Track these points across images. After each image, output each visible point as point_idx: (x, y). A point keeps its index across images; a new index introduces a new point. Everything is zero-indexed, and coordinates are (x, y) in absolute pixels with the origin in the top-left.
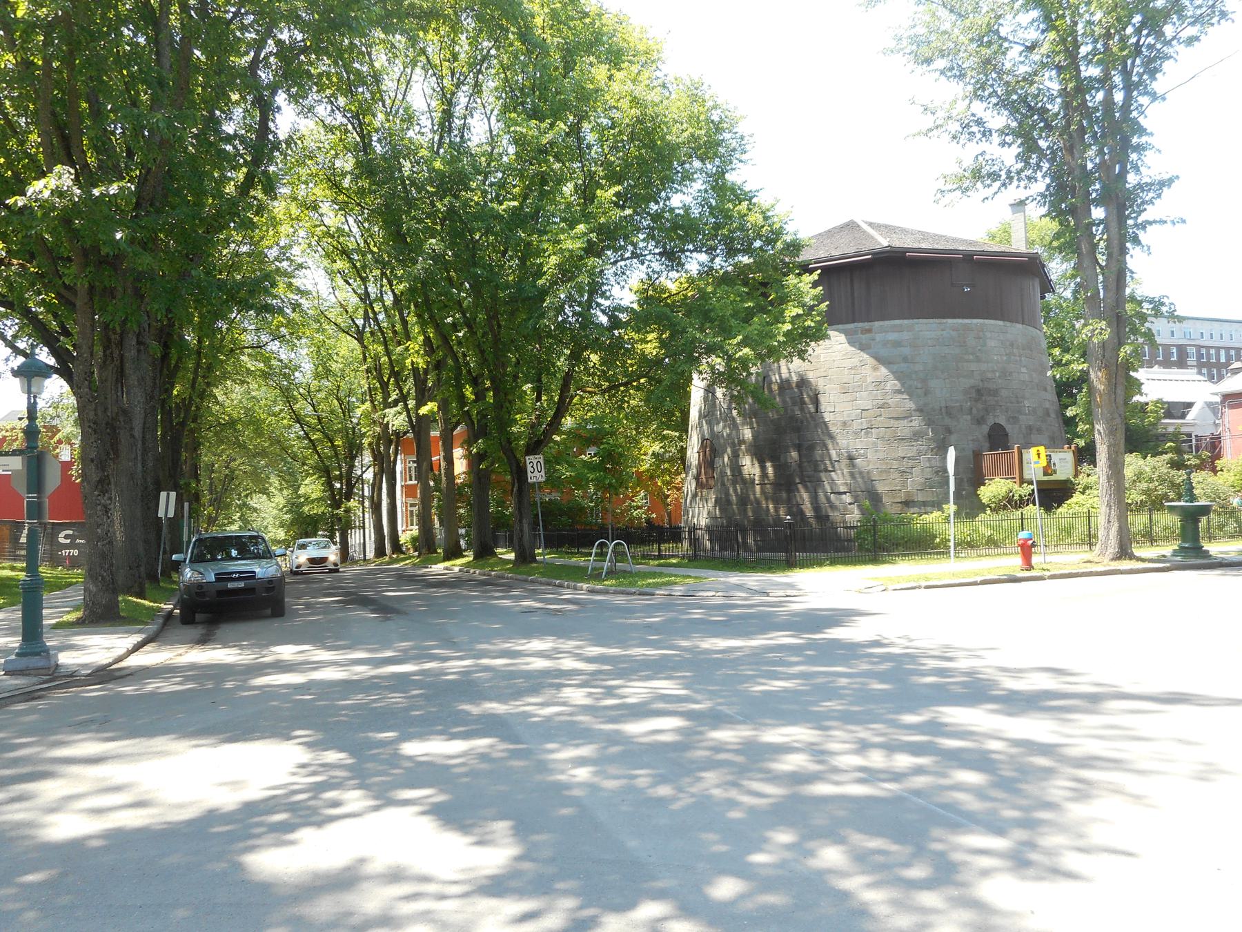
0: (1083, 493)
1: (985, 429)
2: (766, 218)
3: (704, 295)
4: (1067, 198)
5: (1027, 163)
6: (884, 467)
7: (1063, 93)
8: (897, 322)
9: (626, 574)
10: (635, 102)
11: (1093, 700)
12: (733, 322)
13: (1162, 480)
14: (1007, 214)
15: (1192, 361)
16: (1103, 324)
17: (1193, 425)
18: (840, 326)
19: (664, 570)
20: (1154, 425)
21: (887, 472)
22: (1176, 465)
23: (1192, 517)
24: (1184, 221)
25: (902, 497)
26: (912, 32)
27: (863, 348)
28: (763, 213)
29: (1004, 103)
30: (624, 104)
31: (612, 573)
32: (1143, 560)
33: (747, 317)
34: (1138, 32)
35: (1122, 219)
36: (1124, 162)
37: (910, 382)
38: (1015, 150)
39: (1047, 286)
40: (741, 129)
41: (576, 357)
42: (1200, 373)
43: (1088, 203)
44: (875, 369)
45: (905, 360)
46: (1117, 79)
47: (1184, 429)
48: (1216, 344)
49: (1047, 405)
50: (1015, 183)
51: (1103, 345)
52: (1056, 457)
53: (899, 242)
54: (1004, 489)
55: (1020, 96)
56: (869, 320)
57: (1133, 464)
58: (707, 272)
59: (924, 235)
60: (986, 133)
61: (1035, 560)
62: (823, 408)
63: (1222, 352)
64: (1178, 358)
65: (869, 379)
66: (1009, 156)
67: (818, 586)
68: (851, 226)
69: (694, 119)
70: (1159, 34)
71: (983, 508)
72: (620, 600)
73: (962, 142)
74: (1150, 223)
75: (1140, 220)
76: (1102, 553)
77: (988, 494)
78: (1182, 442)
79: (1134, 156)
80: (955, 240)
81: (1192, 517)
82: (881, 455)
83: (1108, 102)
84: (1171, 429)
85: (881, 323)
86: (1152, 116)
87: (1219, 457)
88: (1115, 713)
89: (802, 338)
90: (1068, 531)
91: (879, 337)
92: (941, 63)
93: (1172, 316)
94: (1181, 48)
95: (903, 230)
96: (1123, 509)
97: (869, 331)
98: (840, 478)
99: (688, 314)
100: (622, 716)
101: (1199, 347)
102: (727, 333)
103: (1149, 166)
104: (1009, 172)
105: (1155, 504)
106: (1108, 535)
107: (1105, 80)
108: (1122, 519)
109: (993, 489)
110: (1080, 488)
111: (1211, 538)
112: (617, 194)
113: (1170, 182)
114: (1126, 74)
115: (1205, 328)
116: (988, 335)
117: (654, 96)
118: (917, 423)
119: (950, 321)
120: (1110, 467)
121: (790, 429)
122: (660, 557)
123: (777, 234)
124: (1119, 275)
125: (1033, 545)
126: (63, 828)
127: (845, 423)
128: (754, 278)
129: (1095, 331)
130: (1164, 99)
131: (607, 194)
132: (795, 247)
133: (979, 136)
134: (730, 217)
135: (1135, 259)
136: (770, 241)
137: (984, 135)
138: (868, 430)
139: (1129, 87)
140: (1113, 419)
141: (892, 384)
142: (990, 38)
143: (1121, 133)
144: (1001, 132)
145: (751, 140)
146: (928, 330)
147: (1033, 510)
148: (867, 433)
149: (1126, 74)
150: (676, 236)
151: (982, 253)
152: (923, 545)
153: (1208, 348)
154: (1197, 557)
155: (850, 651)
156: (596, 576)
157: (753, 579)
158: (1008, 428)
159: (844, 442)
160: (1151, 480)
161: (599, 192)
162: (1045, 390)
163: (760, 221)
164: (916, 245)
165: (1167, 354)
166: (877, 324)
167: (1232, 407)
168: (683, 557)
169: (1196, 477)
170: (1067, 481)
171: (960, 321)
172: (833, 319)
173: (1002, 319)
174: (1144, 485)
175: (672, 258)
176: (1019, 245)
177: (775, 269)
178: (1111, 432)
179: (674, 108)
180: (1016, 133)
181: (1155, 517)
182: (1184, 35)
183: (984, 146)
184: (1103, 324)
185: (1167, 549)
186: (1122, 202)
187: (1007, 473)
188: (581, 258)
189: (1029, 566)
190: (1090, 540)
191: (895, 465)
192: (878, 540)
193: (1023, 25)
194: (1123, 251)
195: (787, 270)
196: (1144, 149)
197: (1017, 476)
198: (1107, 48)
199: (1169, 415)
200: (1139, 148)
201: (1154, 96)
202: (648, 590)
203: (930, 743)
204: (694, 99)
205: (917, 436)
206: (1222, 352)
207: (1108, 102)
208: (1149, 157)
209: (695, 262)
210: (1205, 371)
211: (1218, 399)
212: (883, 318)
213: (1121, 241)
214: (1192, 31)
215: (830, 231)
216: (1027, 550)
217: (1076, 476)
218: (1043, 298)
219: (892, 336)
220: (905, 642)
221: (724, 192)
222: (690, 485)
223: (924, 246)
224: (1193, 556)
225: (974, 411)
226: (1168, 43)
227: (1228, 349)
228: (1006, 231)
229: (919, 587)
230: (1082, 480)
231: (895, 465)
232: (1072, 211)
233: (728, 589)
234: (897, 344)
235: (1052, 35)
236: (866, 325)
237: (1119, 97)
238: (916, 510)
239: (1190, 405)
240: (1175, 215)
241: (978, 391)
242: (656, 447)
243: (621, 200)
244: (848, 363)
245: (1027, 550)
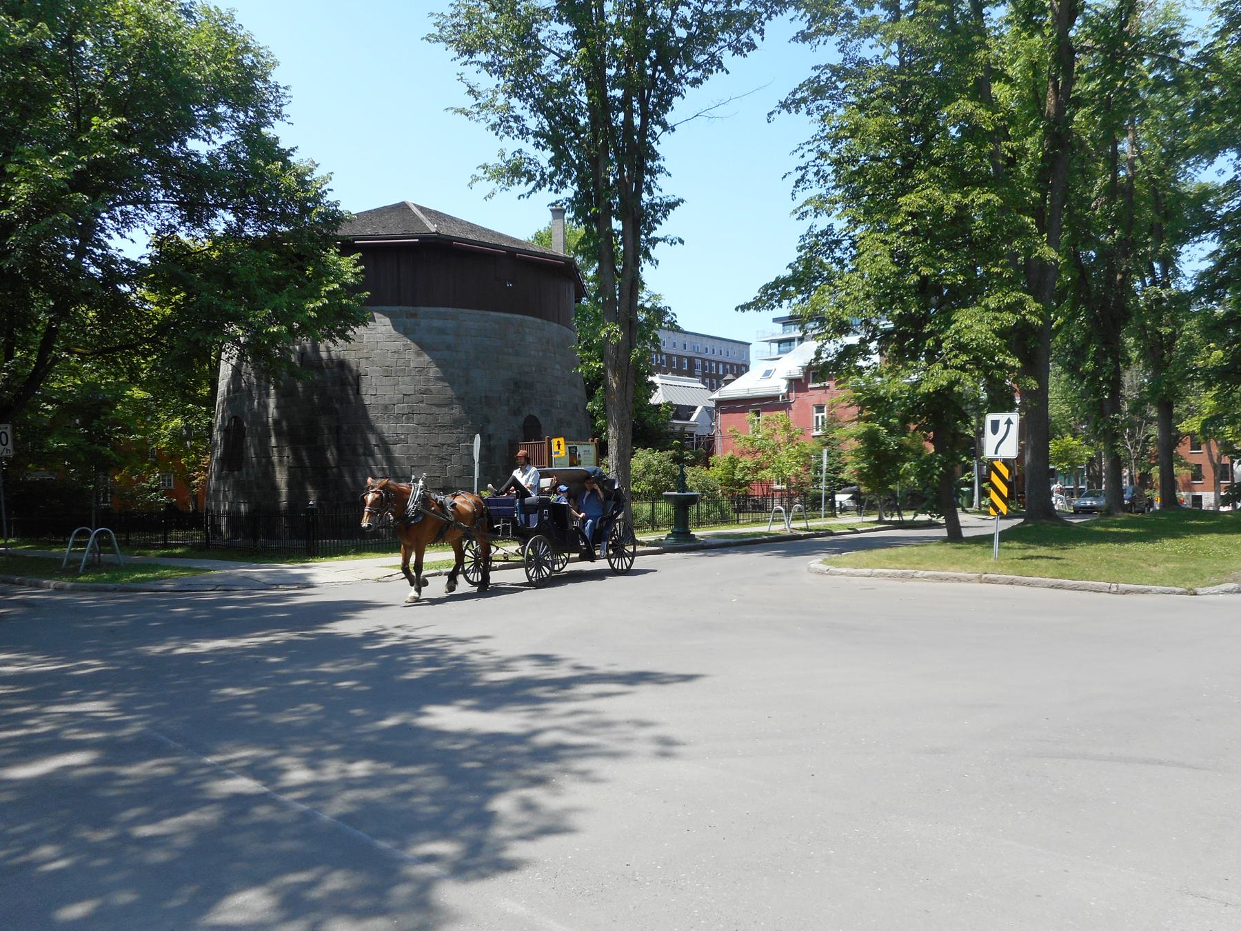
1: (521, 420)
4: (590, 205)
5: (558, 167)
6: (424, 453)
7: (591, 107)
8: (442, 309)
9: (110, 567)
10: (144, 20)
12: (261, 291)
13: (666, 473)
15: (698, 371)
17: (695, 426)
19: (167, 561)
21: (427, 458)
22: (678, 460)
23: (683, 505)
26: (455, 20)
27: (406, 331)
28: (298, 176)
30: (131, 20)
31: (92, 567)
35: (637, 234)
36: (639, 182)
37: (450, 370)
38: (549, 154)
41: (61, 311)
42: (704, 383)
43: (608, 213)
45: (448, 347)
46: (636, 105)
47: (687, 429)
49: (577, 400)
50: (548, 186)
52: (581, 449)
53: (456, 232)
55: (555, 104)
56: (414, 304)
58: (233, 233)
59: (473, 228)
60: (524, 132)
62: (364, 389)
63: (721, 366)
64: (685, 367)
65: (412, 364)
66: (544, 157)
68: (402, 208)
72: (87, 600)
73: (500, 133)
74: (659, 240)
78: (686, 438)
79: (648, 178)
80: (501, 236)
81: (683, 505)
83: (628, 121)
84: (677, 429)
85: (427, 309)
86: (665, 145)
87: (711, 453)
89: (341, 318)
91: (423, 323)
97: (414, 315)
99: (206, 277)
100: (11, 755)
101: (704, 360)
102: (255, 304)
103: (664, 187)
104: (543, 174)
107: (625, 103)
111: (698, 524)
112: (120, 126)
114: (644, 102)
118: (457, 411)
119: (492, 313)
120: (618, 459)
121: (328, 412)
122: (166, 546)
124: (635, 284)
127: (386, 407)
129: (611, 331)
130: (673, 130)
132: (334, 218)
133: (516, 132)
134: (262, 175)
135: (647, 272)
137: (521, 132)
138: (409, 416)
139: (645, 116)
140: (622, 415)
141: (434, 371)
142: (525, 37)
143: (639, 157)
144: (536, 135)
146: (472, 320)
148: (408, 419)
149: (644, 102)
150: (196, 190)
151: (526, 252)
153: (711, 361)
154: (685, 541)
155: (347, 645)
156: (72, 570)
158: (542, 420)
160: (657, 472)
162: (575, 386)
164: (463, 235)
165: (670, 363)
166: (422, 309)
167: (723, 412)
169: (689, 471)
171: (502, 314)
172: (378, 301)
173: (540, 317)
174: (652, 477)
175: (195, 213)
176: (558, 249)
177: (311, 238)
178: (621, 428)
180: (550, 140)
181: (657, 505)
185: (663, 534)
186: (641, 220)
188: (64, 192)
191: (435, 451)
193: (556, 35)
194: (637, 263)
195: (327, 242)
199: (677, 417)
200: (652, 172)
201: (665, 127)
202: (133, 586)
204: (222, 35)
205: (456, 423)
206: (721, 366)
207: (628, 121)
208: (661, 179)
209: (222, 221)
210: (707, 381)
211: (713, 405)
212: (428, 304)
213: (638, 251)
214: (698, 74)
218: (579, 301)
219: (437, 323)
220: (403, 633)
223: (470, 237)
225: (511, 402)
226: (678, 81)
227: (725, 364)
231: (435, 451)
232: (596, 219)
234: (441, 331)
235: (583, 50)
236: (411, 309)
237: (637, 121)
239: (694, 408)
240: (674, 235)
241: (516, 383)
244: (392, 346)
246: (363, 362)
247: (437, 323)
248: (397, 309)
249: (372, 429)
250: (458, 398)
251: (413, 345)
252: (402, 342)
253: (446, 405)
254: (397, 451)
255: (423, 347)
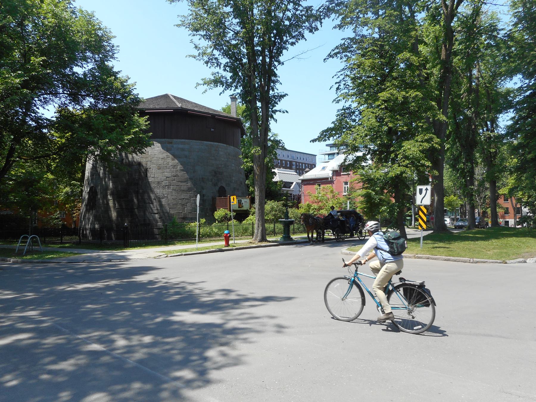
0: (253, 215)
1: (217, 188)
2: (123, 86)
3: (89, 117)
4: (248, 96)
8: (183, 140)
9: (37, 252)
10: (55, 15)
11: (236, 303)
13: (280, 211)
14: (229, 101)
15: (294, 167)
16: (259, 148)
17: (293, 191)
18: (158, 140)
20: (280, 190)
21: (176, 204)
23: (287, 225)
24: (287, 112)
25: (182, 216)
27: (168, 150)
29: (226, 54)
32: (270, 242)
33: (112, 129)
34: (275, 37)
35: (267, 108)
36: (269, 86)
39: (243, 133)
40: (113, 42)
41: (17, 140)
42: (296, 172)
44: (173, 160)
45: (186, 157)
46: (267, 53)
47: (289, 192)
48: (302, 162)
51: (259, 156)
52: (243, 201)
53: (189, 107)
54: (224, 214)
56: (171, 138)
57: (270, 205)
58: (93, 107)
59: (197, 105)
61: (231, 242)
62: (149, 175)
63: (304, 165)
64: (288, 165)
66: (228, 75)
67: (138, 256)
68: (166, 96)
69: (88, 32)
70: (282, 39)
71: (215, 220)
75: (274, 109)
76: (255, 239)
77: (218, 215)
80: (209, 109)
81: (287, 225)
82: (174, 197)
84: (285, 192)
85: (176, 140)
86: (279, 70)
87: (300, 203)
88: (246, 310)
89: (139, 144)
90: (246, 230)
91: (175, 146)
92: (202, 33)
93: (284, 149)
94: (289, 46)
95: (188, 101)
96: (263, 221)
97: (171, 143)
98: (155, 207)
101: (296, 162)
105: (275, 220)
106: (258, 231)
107: (262, 53)
108: (263, 226)
109: (219, 213)
110: (251, 213)
111: (294, 233)
112: (43, 61)
113: (285, 96)
114: (270, 52)
115: (299, 155)
116: (220, 149)
117: (66, 15)
118: (189, 184)
119: (205, 142)
121: (133, 183)
123: (129, 93)
124: (267, 129)
125: (230, 236)
126: (388, 247)
127: (159, 183)
128: (116, 113)
129: (256, 150)
130: (283, 64)
131: (37, 60)
132: (137, 101)
133: (216, 65)
135: (272, 124)
136: (124, 97)
137: (218, 65)
138: (169, 186)
141: (179, 167)
143: (269, 75)
145: (118, 48)
146: (196, 145)
147: (234, 222)
148: (168, 187)
150: (77, 88)
152: (189, 237)
153: (299, 163)
155: (142, 286)
156: (20, 253)
157: (104, 254)
158: (226, 188)
159: (158, 191)
160: (276, 211)
161: (32, 58)
162: (241, 173)
163: (120, 86)
164: (192, 108)
165: (282, 164)
166: (175, 140)
168: (74, 243)
169: (290, 210)
170: (247, 210)
172: (155, 137)
174: (274, 213)
175: (75, 98)
176: (233, 115)
178: (261, 191)
179: (77, 25)
181: (276, 225)
182: (291, 41)
183: (217, 69)
184: (259, 148)
185: (279, 238)
186: (269, 102)
187: (225, 207)
189: (227, 244)
190: (252, 234)
191: (180, 202)
192: (171, 233)
194: (267, 120)
196: (276, 82)
197: (228, 208)
198: (264, 39)
199: (285, 187)
200: (274, 82)
201: (279, 63)
203: (166, 329)
204: (89, 22)
205: (189, 190)
206: (304, 165)
208: (278, 85)
209: (88, 102)
211: (300, 181)
213: (268, 116)
214: (294, 40)
215: (156, 97)
216: (227, 239)
217: (250, 208)
219: (181, 146)
221: (105, 71)
222: (82, 207)
224: (287, 241)
225: (213, 180)
227: (305, 164)
228: (229, 108)
229: (182, 255)
230: (253, 210)
231: (180, 202)
233: (91, 260)
234: (183, 150)
236: (170, 140)
237: (268, 60)
238: (188, 221)
239: (292, 183)
240: (284, 109)
241: (215, 172)
242: (68, 189)
243: (45, 65)
244: (161, 156)
245: (227, 239)
246: (149, 163)
247: (181, 146)
248: (163, 140)
249: (153, 192)
250: (190, 179)
251: (170, 156)
252: (166, 154)
253: (185, 182)
254: (164, 201)
255: (175, 156)
